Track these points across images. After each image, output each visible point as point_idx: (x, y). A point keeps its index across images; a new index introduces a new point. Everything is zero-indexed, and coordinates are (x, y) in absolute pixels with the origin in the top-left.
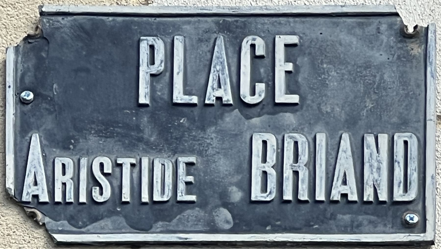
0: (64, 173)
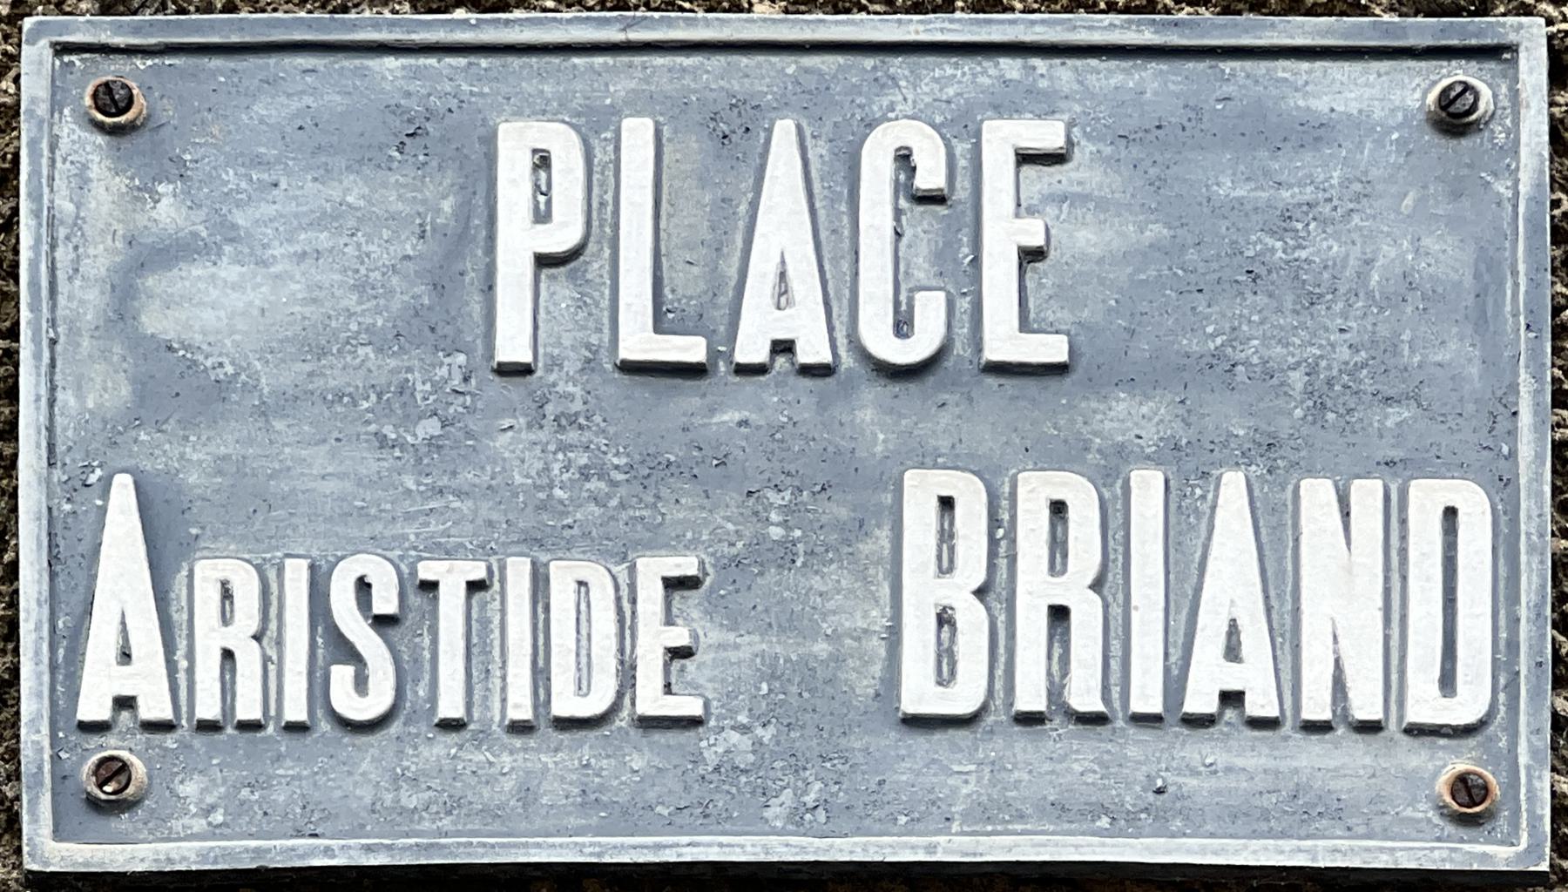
0: (226, 620)
